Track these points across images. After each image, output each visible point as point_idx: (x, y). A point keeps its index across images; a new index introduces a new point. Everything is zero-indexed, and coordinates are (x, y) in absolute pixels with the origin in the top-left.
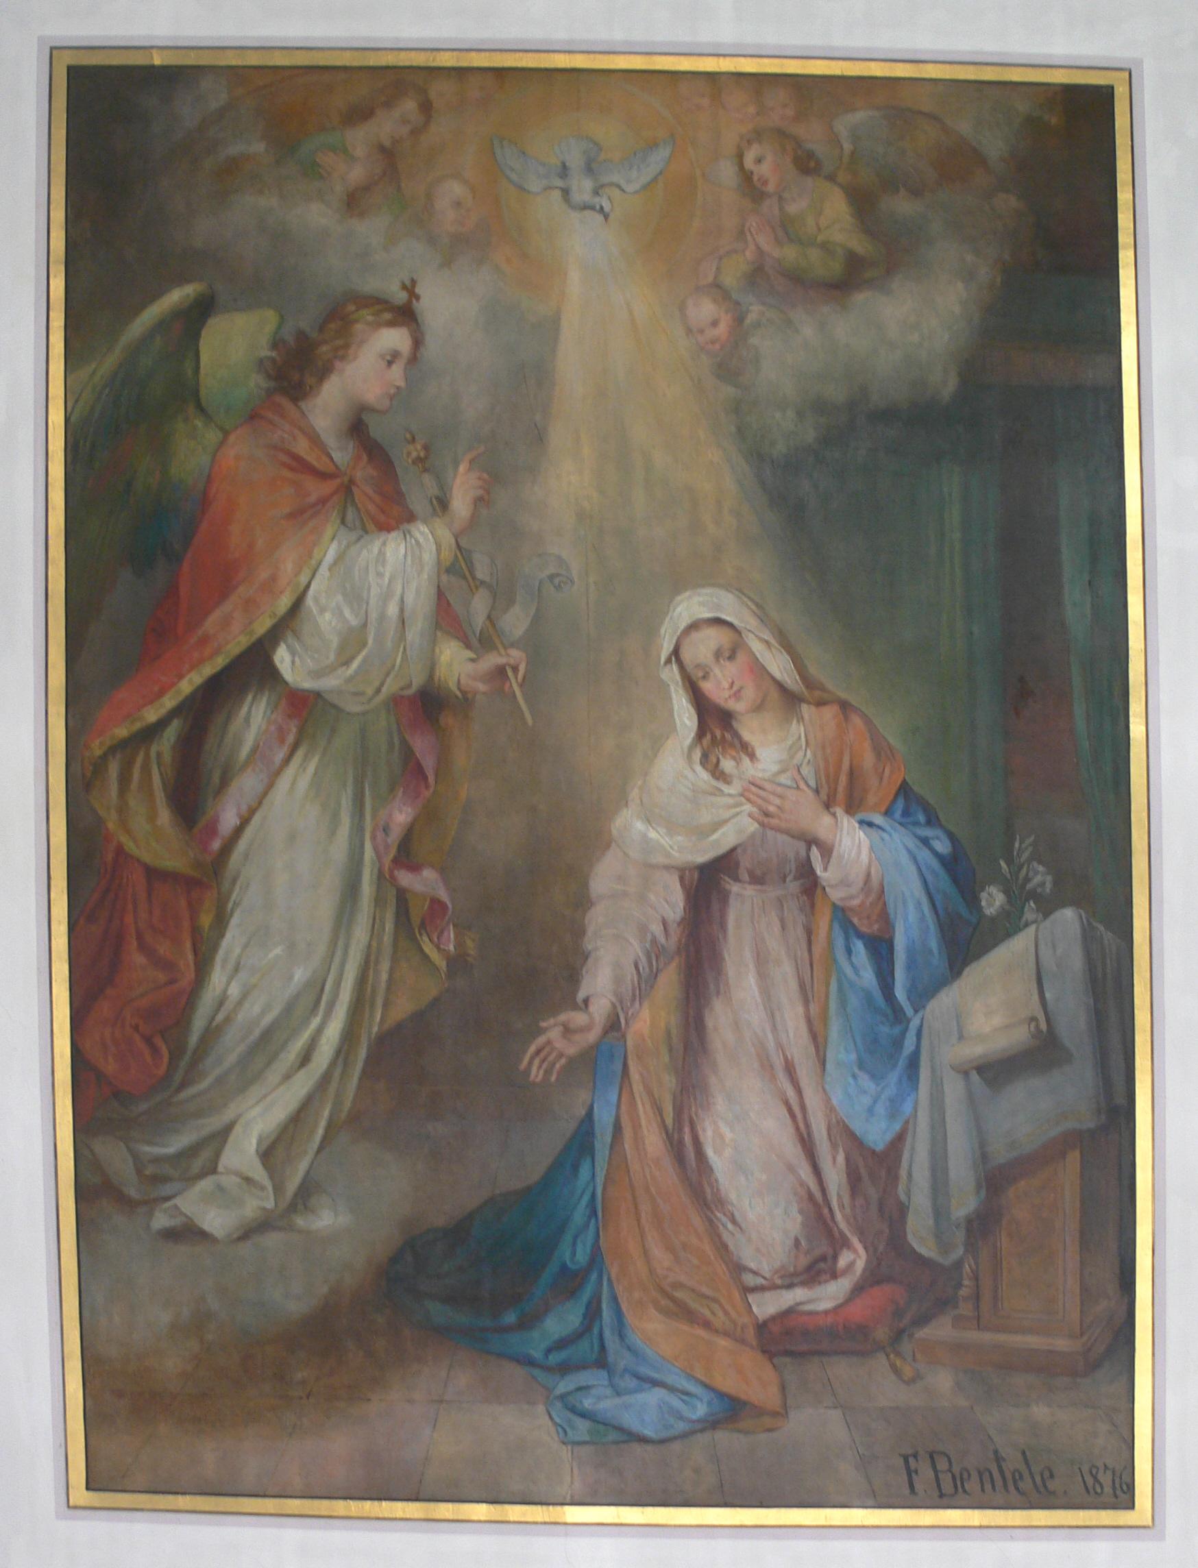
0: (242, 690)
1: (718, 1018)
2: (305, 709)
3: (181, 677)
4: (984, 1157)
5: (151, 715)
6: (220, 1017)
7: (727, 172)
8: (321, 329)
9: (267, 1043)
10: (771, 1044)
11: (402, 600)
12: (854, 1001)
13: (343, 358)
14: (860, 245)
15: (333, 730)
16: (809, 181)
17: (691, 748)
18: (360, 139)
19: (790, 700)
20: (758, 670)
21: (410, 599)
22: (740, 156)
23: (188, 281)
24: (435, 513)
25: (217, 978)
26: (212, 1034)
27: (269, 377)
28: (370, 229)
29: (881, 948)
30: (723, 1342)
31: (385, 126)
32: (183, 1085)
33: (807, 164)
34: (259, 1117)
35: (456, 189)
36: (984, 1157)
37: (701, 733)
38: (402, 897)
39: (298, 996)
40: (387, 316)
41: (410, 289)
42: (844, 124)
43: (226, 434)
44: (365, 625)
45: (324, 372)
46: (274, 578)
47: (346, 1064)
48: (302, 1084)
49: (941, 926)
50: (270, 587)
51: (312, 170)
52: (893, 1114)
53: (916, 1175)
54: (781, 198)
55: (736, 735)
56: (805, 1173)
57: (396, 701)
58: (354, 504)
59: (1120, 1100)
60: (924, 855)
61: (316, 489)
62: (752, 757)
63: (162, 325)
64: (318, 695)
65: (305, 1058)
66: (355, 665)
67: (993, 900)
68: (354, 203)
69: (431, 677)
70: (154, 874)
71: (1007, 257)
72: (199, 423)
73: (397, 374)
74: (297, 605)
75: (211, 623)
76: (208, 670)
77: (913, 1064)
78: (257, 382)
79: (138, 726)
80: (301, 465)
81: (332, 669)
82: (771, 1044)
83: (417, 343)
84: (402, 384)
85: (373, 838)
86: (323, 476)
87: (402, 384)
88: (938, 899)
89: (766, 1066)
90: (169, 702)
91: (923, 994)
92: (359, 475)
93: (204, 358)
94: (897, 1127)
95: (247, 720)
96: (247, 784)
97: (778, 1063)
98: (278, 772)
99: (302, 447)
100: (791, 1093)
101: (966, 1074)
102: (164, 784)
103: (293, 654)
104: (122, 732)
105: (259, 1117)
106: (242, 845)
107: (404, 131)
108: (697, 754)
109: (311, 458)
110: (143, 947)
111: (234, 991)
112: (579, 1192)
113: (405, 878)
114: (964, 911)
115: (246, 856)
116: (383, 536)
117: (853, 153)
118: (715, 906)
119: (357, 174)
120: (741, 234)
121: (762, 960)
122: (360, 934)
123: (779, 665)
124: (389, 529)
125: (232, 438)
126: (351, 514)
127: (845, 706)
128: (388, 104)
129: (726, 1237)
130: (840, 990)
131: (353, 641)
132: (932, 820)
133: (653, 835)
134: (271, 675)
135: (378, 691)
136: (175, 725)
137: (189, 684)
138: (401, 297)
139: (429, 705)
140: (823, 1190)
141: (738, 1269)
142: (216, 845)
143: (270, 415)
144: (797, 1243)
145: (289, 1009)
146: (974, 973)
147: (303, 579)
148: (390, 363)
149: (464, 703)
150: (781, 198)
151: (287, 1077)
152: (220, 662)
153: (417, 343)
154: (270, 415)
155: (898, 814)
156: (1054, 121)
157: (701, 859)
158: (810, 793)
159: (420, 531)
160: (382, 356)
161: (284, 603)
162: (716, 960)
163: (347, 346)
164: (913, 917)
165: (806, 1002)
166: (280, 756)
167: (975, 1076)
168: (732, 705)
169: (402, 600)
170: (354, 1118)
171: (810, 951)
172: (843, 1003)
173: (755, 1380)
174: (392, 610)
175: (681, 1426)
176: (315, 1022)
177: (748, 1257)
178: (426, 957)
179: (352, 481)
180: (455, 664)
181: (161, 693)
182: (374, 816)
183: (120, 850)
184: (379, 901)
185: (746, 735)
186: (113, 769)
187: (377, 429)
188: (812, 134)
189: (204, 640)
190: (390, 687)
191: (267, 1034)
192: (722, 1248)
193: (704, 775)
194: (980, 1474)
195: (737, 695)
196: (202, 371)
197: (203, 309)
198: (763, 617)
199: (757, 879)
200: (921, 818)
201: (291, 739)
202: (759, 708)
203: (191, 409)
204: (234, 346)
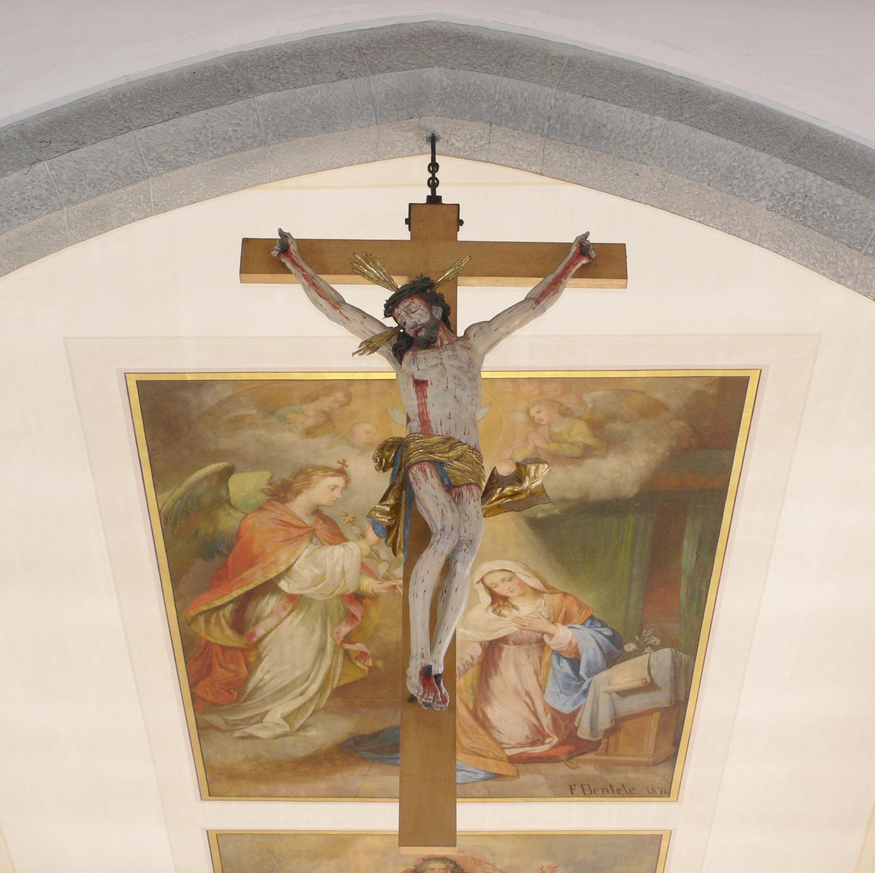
0: (264, 595)
1: (496, 683)
2: (295, 601)
3: (232, 591)
4: (615, 714)
5: (218, 603)
6: (261, 684)
7: (521, 417)
8: (295, 478)
9: (282, 692)
10: (520, 688)
11: (343, 566)
12: (559, 676)
13: (307, 488)
14: (590, 441)
15: (310, 606)
16: (566, 419)
17: (487, 608)
18: (311, 409)
19: (537, 593)
20: (521, 584)
21: (347, 566)
22: (528, 413)
23: (220, 461)
24: (359, 539)
25: (258, 674)
26: (256, 689)
27: (268, 495)
28: (321, 442)
29: (575, 663)
30: (491, 761)
31: (325, 403)
32: (244, 702)
33: (565, 413)
34: (277, 712)
35: (368, 427)
36: (615, 714)
37: (493, 603)
38: (347, 653)
39: (297, 679)
40: (331, 473)
41: (343, 463)
42: (588, 398)
43: (247, 514)
44: (325, 574)
45: (299, 493)
46: (277, 561)
47: (321, 695)
48: (300, 701)
49: (604, 655)
50: (275, 563)
51: (284, 420)
52: (574, 704)
53: (583, 718)
54: (549, 426)
55: (510, 603)
56: (533, 720)
57: (342, 596)
58: (316, 536)
59: (682, 699)
60: (599, 637)
61: (295, 532)
62: (517, 609)
63: (207, 478)
64: (302, 596)
65: (302, 694)
66: (320, 586)
67: (630, 647)
68: (310, 432)
69: (359, 586)
70: (224, 648)
71: (674, 444)
72: (231, 511)
73: (337, 493)
74: (289, 569)
75: (245, 575)
76: (246, 589)
77: (585, 692)
78: (262, 498)
79: (211, 606)
80: (288, 524)
81: (309, 588)
82: (520, 688)
83: (347, 482)
84: (340, 496)
85: (332, 635)
86: (300, 528)
87: (340, 496)
88: (604, 648)
89: (517, 693)
90: (226, 599)
91: (591, 673)
92: (318, 527)
93: (231, 489)
94: (576, 707)
95: (267, 604)
96: (269, 622)
97: (523, 693)
98: (284, 618)
99: (288, 519)
100: (528, 700)
101: (610, 693)
102: (228, 623)
103: (289, 583)
104: (205, 608)
105: (277, 712)
106: (267, 639)
107: (336, 405)
108: (491, 609)
109: (294, 522)
110: (221, 666)
111: (267, 677)
112: (246, 694)
113: (348, 646)
114: (616, 650)
115: (270, 642)
116: (333, 547)
117: (592, 408)
118: (496, 652)
119: (310, 422)
120: (526, 440)
121: (517, 666)
122: (327, 662)
123: (534, 583)
124: (336, 544)
125: (250, 516)
126: (315, 540)
127: (565, 594)
128: (327, 395)
129: (497, 737)
130: (554, 672)
131: (316, 581)
132: (604, 625)
133: (467, 632)
134: (277, 590)
135: (332, 593)
136: (230, 608)
137: (236, 594)
138: (338, 466)
139: (358, 597)
140: (540, 724)
141: (500, 744)
142: (255, 639)
143: (270, 508)
144: (527, 737)
145: (294, 682)
146: (616, 668)
147: (292, 561)
148: (333, 490)
149: (375, 597)
150: (549, 426)
151: (294, 698)
152: (251, 587)
153: (347, 482)
154: (270, 508)
155: (587, 625)
156: (711, 392)
157: (490, 639)
158: (546, 620)
159: (351, 545)
160: (329, 487)
161: (283, 568)
162: (495, 665)
163: (309, 484)
164: (591, 652)
165: (537, 676)
166: (284, 614)
167: (615, 695)
168: (508, 595)
169: (343, 566)
170: (326, 709)
171: (540, 661)
172: (555, 676)
173: (506, 769)
174: (338, 569)
175: (472, 780)
176: (306, 685)
177: (504, 740)
178: (358, 667)
179: (314, 529)
180: (369, 584)
181: (223, 596)
182: (332, 629)
183: (207, 642)
184: (335, 652)
185: (515, 603)
186: (201, 620)
187: (326, 512)
188: (570, 401)
189: (242, 580)
190: (338, 592)
191: (284, 688)
192: (493, 739)
193: (493, 616)
194: (603, 790)
195: (512, 592)
196: (231, 494)
197: (230, 471)
198: (527, 568)
199: (515, 643)
200: (599, 625)
201: (290, 609)
202: (522, 595)
203: (227, 506)
204: (246, 486)
